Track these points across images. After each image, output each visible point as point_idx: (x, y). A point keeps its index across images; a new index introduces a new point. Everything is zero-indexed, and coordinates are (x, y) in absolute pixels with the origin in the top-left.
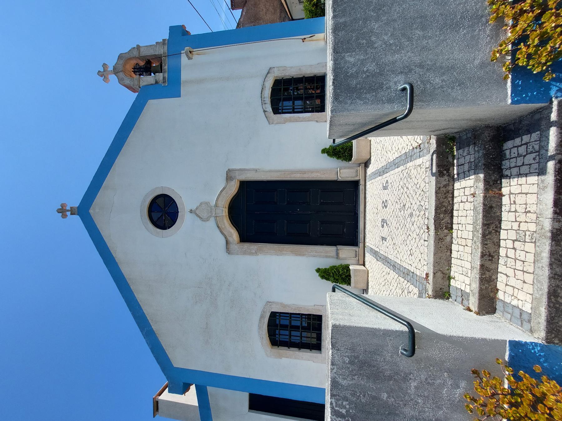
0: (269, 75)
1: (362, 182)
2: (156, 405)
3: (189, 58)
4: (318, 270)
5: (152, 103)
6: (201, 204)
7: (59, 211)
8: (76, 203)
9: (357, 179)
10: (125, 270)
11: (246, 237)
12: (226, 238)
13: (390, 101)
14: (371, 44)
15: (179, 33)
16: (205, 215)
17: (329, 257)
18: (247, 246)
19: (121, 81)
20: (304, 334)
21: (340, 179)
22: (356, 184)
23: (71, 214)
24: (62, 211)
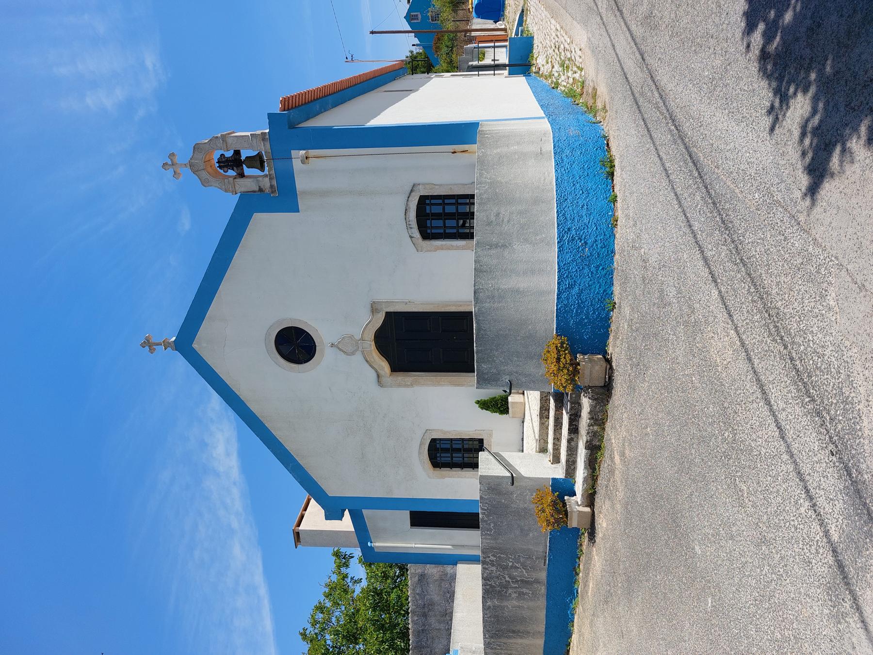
0: (413, 194)
2: (297, 536)
4: (478, 402)
10: (254, 407)
11: (397, 367)
12: (376, 371)
14: (494, 361)
18: (401, 377)
20: (466, 455)
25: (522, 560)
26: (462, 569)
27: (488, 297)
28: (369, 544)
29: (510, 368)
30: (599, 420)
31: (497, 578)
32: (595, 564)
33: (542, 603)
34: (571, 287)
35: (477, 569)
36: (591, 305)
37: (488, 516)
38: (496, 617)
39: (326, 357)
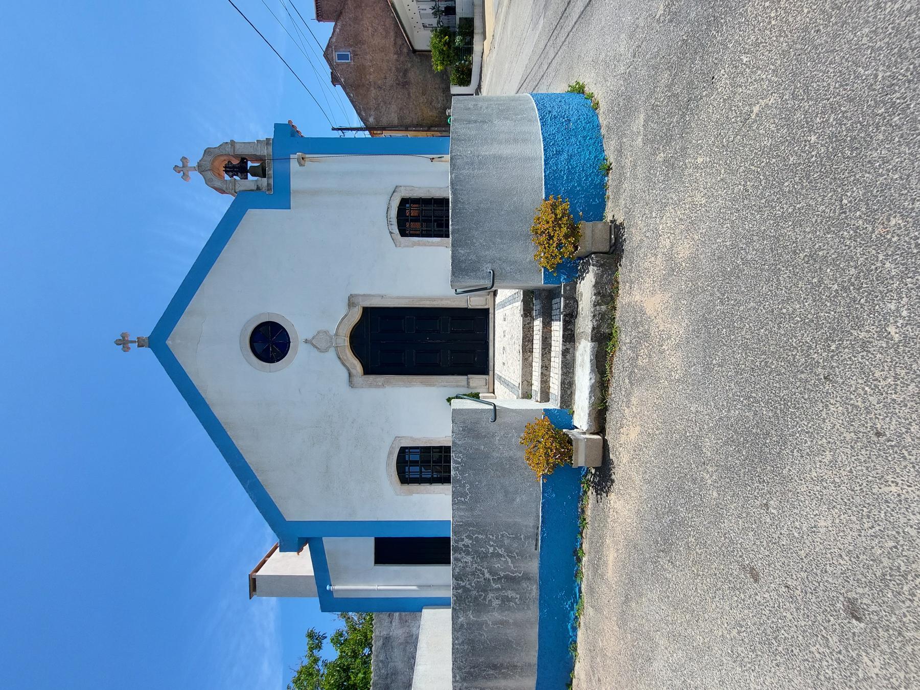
1: (491, 311)
3: (301, 165)
5: (254, 216)
6: (319, 332)
7: (118, 343)
8: (146, 333)
9: (486, 307)
10: (218, 412)
12: (348, 370)
13: (483, 278)
15: (287, 136)
16: (322, 345)
17: (460, 386)
19: (208, 182)
21: (470, 307)
22: (486, 311)
23: (139, 346)
24: (123, 342)
25: (506, 542)
26: (427, 614)
27: (467, 163)
28: (328, 588)
29: (491, 253)
30: (607, 295)
31: (473, 574)
32: (616, 520)
33: (533, 613)
34: (559, 153)
35: (446, 614)
36: (583, 170)
37: (462, 472)
38: (471, 642)
39: (299, 354)
